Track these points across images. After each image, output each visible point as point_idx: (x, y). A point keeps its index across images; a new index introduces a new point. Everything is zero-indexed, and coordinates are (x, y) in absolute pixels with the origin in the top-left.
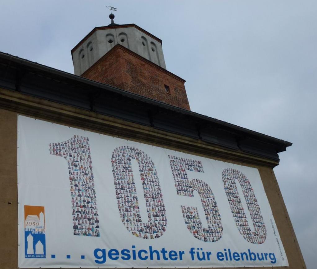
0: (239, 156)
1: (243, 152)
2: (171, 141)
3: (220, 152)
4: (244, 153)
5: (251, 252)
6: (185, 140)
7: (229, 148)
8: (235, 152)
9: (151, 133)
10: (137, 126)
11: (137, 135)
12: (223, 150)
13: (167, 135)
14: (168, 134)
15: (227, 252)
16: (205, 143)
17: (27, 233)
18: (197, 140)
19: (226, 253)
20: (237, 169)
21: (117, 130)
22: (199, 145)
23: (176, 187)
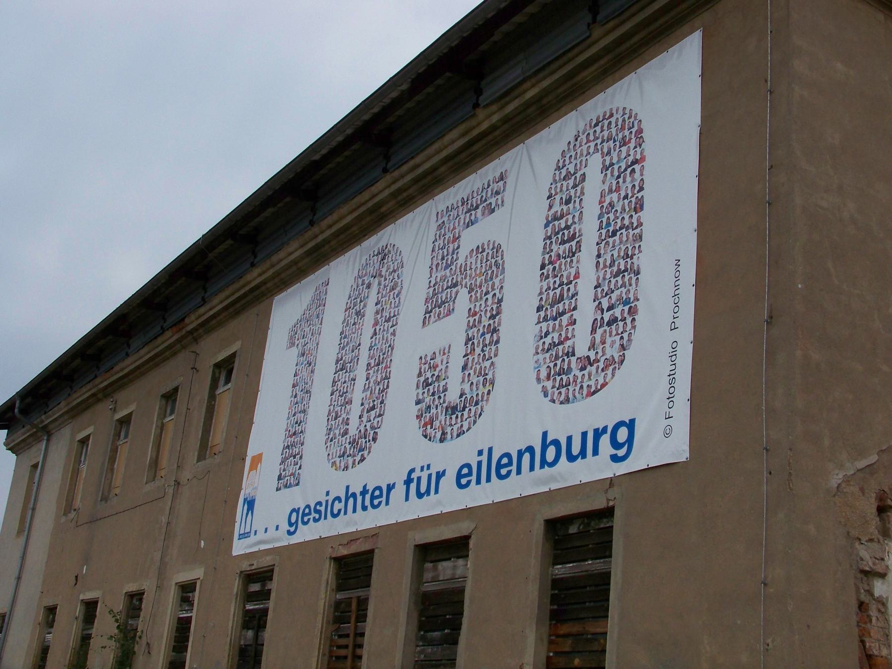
0: (607, 50)
1: (611, 24)
2: (434, 169)
3: (546, 92)
4: (616, 21)
5: (549, 440)
6: (453, 142)
7: (564, 54)
8: (589, 47)
9: (394, 187)
10: (366, 195)
11: (384, 209)
12: (545, 83)
13: (417, 166)
14: (417, 160)
15: (484, 458)
16: (494, 107)
17: (245, 500)
18: (474, 115)
19: (480, 463)
20: (600, 112)
21: (355, 228)
22: (485, 126)
23: (540, 386)
